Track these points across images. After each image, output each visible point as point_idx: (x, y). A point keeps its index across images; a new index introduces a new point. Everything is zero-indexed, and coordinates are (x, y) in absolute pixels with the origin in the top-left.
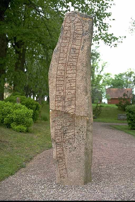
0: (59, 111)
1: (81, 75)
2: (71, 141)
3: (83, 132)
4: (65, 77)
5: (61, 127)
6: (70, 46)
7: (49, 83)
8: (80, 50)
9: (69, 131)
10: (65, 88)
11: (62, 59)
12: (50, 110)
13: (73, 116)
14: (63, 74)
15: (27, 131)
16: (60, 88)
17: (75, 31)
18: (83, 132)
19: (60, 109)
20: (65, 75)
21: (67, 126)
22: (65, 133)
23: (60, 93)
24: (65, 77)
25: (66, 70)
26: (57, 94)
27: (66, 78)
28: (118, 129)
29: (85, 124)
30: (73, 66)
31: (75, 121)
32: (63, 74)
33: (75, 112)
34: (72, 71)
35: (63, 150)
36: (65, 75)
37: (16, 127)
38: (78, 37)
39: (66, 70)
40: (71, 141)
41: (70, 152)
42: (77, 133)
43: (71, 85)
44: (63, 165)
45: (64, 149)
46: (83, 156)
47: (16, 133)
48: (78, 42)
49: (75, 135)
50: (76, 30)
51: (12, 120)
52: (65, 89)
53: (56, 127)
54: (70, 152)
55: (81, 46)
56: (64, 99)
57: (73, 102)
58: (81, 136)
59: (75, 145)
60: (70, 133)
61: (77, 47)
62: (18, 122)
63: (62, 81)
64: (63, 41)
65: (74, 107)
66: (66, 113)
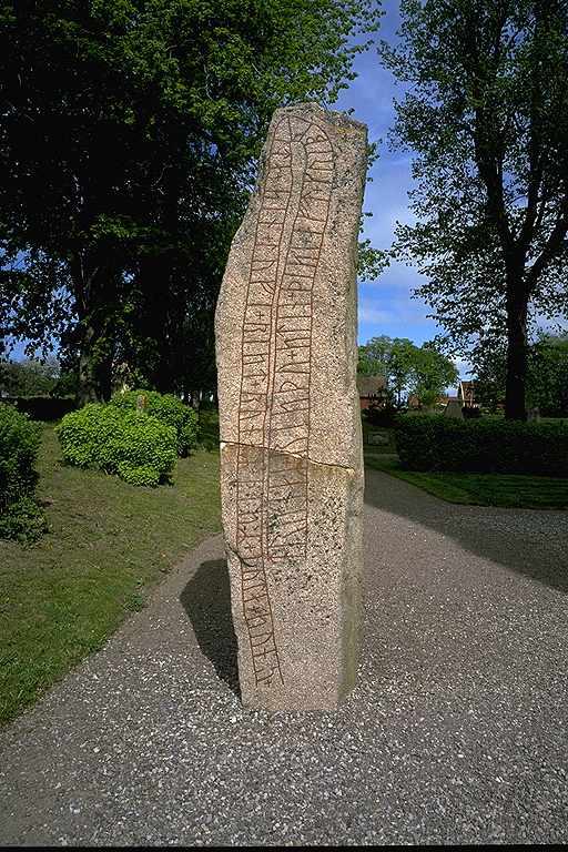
0: (253, 446)
1: (329, 322)
2: (293, 551)
3: (334, 521)
4: (274, 328)
5: (258, 502)
6: (288, 220)
7: (218, 349)
8: (327, 239)
9: (286, 518)
10: (272, 366)
12: (222, 445)
13: (301, 465)
14: (266, 320)
15: (164, 479)
16: (256, 368)
18: (334, 521)
19: (256, 439)
20: (274, 321)
21: (279, 501)
22: (274, 524)
23: (256, 384)
24: (274, 328)
26: (245, 389)
27: (277, 331)
28: (378, 469)
29: (343, 491)
30: (300, 290)
31: (307, 483)
32: (266, 320)
33: (307, 451)
34: (297, 310)
35: (265, 585)
36: (274, 321)
37: (130, 473)
38: (318, 190)
40: (293, 551)
41: (291, 591)
42: (316, 523)
44: (267, 636)
45: (270, 581)
46: (335, 606)
47: (130, 489)
48: (318, 210)
49: (307, 532)
50: (311, 168)
51: (121, 455)
53: (242, 504)
54: (291, 591)
55: (330, 224)
56: (269, 407)
57: (300, 415)
58: (330, 535)
59: (308, 566)
60: (290, 526)
61: (314, 226)
62: (138, 460)
64: (267, 205)
65: (306, 435)
66: (277, 455)
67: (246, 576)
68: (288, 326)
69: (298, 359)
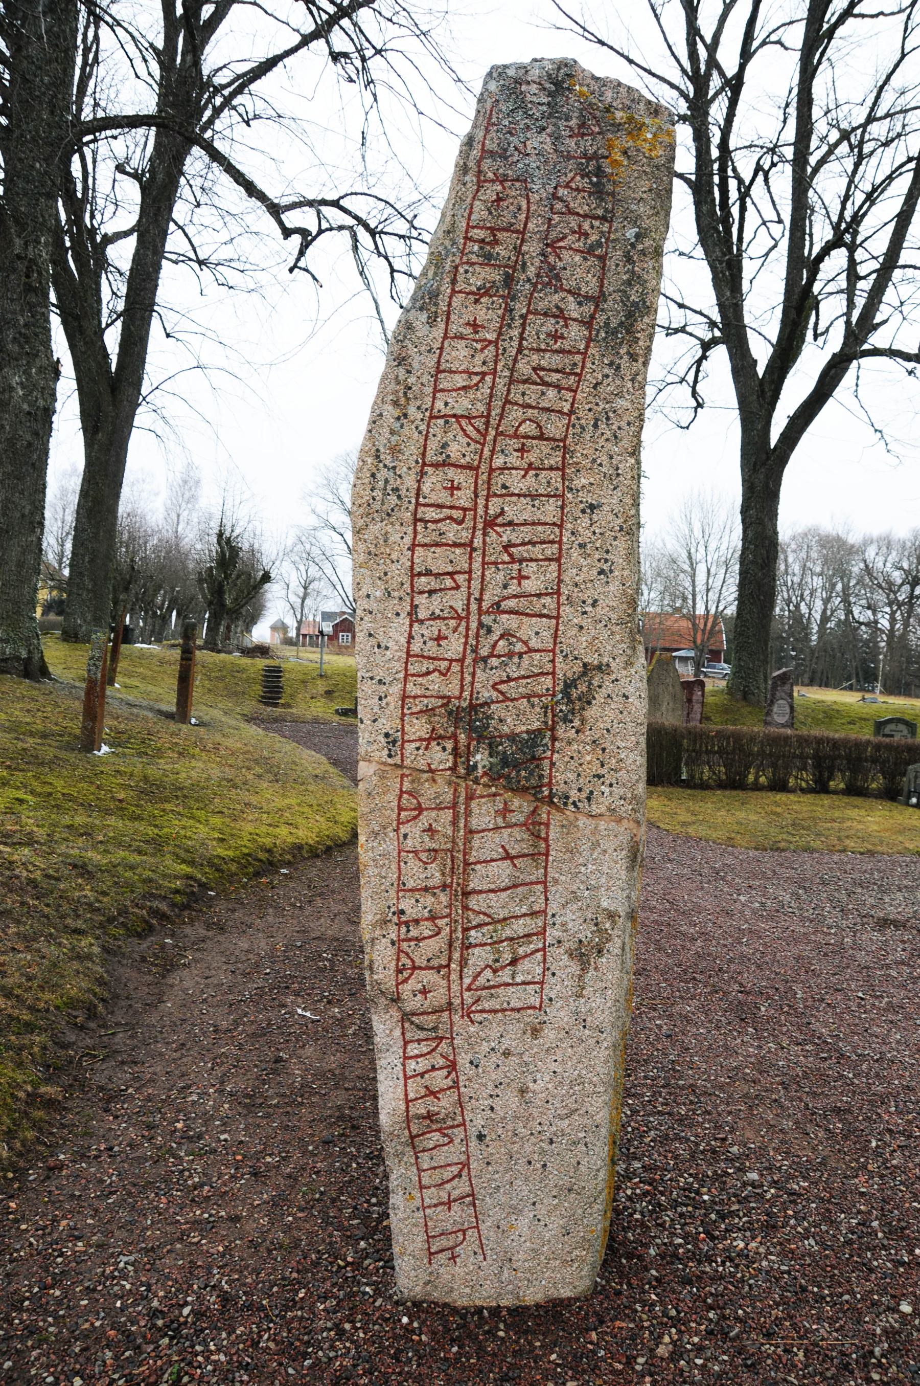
0: (431, 771)
11: (460, 381)
14: (464, 498)
17: (562, 192)
20: (481, 502)
25: (484, 468)
26: (416, 648)
32: (464, 498)
35: (452, 1066)
36: (481, 502)
39: (484, 468)
43: (521, 577)
52: (474, 607)
63: (455, 545)
67: (413, 1049)
68: (516, 510)
69: (530, 586)
